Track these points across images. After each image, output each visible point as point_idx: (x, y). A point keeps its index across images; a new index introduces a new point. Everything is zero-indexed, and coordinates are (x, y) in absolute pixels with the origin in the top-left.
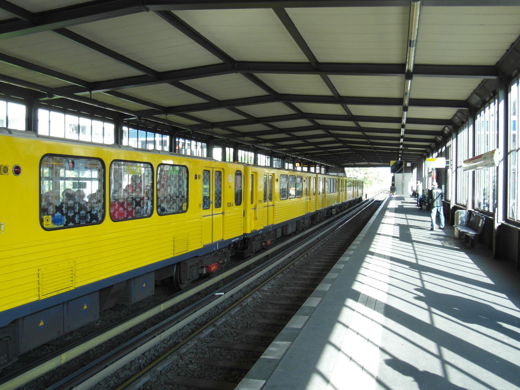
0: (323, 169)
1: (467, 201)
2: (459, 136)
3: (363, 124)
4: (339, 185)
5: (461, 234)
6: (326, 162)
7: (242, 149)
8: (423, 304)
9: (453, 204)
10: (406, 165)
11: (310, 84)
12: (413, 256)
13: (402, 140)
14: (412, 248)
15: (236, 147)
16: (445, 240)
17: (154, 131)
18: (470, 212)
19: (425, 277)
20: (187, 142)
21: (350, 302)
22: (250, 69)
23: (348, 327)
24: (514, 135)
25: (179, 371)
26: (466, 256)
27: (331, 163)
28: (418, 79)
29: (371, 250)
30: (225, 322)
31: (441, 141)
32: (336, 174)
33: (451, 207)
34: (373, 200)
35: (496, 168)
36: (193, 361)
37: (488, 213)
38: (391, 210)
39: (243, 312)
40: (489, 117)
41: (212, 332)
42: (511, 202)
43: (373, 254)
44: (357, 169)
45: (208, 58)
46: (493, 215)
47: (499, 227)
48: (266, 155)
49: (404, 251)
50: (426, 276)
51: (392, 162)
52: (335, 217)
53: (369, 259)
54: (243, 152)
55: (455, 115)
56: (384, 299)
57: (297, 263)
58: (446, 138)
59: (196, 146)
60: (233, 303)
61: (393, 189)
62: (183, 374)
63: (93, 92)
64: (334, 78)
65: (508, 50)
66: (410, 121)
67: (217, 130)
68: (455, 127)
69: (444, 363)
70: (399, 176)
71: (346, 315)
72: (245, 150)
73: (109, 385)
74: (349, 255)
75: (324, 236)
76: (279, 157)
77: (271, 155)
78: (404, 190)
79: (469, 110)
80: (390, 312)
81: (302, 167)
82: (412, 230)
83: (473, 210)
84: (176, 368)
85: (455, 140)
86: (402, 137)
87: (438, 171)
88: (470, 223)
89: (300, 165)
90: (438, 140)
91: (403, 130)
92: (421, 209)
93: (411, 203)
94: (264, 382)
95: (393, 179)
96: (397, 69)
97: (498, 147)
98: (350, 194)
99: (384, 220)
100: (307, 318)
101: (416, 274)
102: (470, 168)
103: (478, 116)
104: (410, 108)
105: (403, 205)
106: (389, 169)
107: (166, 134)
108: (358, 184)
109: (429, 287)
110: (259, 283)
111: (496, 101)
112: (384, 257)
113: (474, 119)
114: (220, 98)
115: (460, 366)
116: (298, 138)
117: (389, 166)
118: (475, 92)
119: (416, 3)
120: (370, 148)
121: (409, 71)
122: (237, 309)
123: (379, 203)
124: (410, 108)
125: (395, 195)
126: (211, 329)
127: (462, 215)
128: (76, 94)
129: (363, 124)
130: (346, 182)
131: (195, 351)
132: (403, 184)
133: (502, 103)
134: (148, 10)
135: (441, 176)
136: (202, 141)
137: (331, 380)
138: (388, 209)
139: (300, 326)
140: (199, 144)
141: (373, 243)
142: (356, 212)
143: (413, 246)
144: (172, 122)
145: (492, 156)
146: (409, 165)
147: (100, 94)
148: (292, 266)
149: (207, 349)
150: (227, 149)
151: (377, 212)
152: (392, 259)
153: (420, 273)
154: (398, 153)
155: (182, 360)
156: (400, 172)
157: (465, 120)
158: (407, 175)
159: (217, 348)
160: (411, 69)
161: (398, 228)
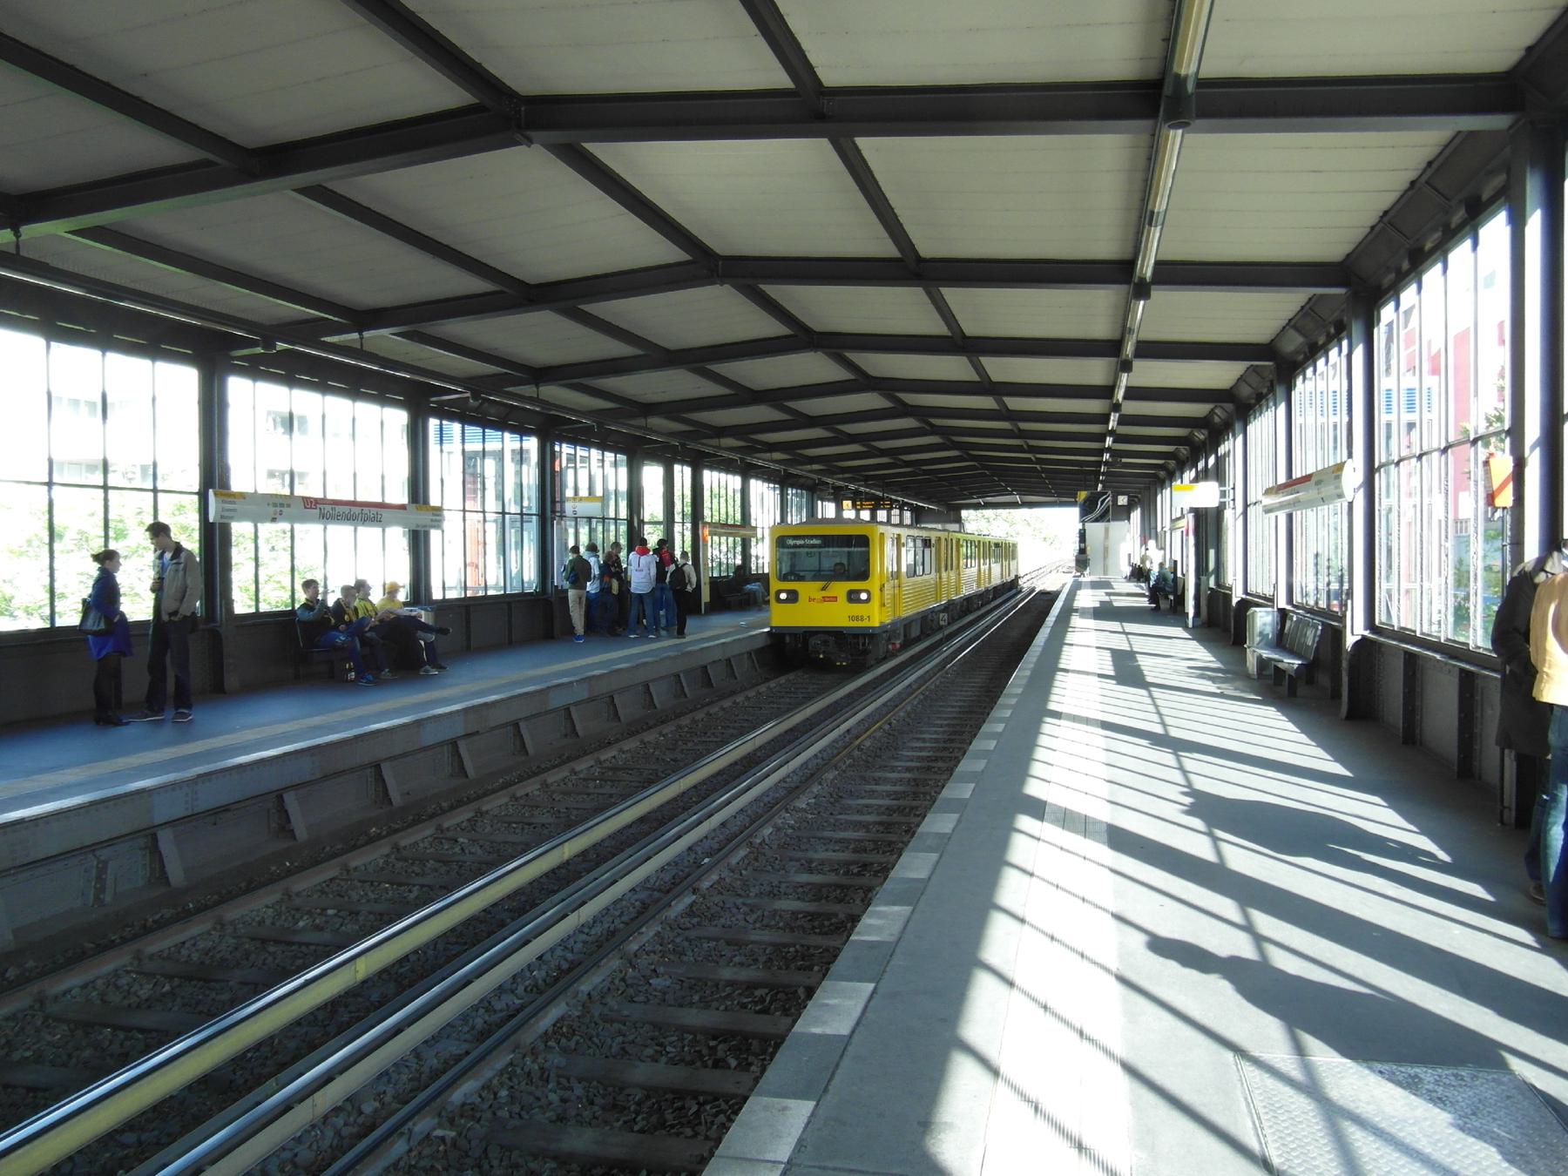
0: (907, 515)
1: (1276, 586)
2: (1250, 428)
3: (1014, 403)
4: (942, 555)
5: (1263, 663)
6: (917, 497)
7: (712, 468)
8: (1197, 823)
9: (1237, 595)
10: (1115, 500)
11: (899, 309)
12: (1156, 718)
13: (1109, 441)
14: (1149, 701)
15: (698, 463)
16: (1224, 681)
17: (501, 425)
18: (1283, 614)
19: (1189, 764)
20: (581, 452)
21: (1025, 822)
22: (751, 274)
23: (1032, 875)
24: (1389, 425)
25: (631, 991)
26: (1278, 715)
27: (928, 500)
28: (1161, 296)
29: (1052, 706)
30: (718, 882)
31: (1204, 443)
32: (939, 526)
33: (1235, 601)
34: (1033, 590)
35: (1345, 505)
36: (661, 970)
37: (1326, 614)
38: (1084, 613)
39: (756, 859)
40: (1324, 384)
41: (691, 905)
42: (1382, 587)
43: (1057, 715)
44: (989, 513)
45: (657, 250)
46: (1342, 619)
47: (1357, 644)
48: (768, 480)
49: (1130, 706)
50: (1192, 762)
51: (1083, 495)
52: (947, 632)
53: (1049, 726)
54: (715, 474)
55: (1241, 379)
56: (1104, 814)
57: (868, 744)
58: (1217, 433)
59: (603, 461)
60: (729, 841)
61: (1082, 561)
62: (641, 998)
63: (366, 334)
64: (954, 296)
65: (1373, 228)
66: (1133, 393)
67: (656, 422)
68: (1237, 408)
69: (1259, 939)
70: (1095, 529)
71: (1021, 849)
72: (720, 470)
73: (473, 1028)
74: (1000, 720)
75: (923, 680)
76: (801, 487)
77: (783, 481)
78: (1110, 562)
79: (1275, 368)
80: (1120, 840)
81: (858, 511)
82: (1143, 661)
83: (1289, 607)
84: (622, 986)
85: (1240, 439)
86: (1112, 433)
87: (1200, 515)
88: (1281, 640)
89: (854, 506)
90: (1200, 436)
91: (1114, 417)
92: (1157, 609)
93: (1133, 595)
94: (871, 986)
95: (1083, 536)
96: (1119, 272)
97: (1350, 455)
98: (973, 576)
99: (1070, 637)
100: (934, 856)
101: (1167, 757)
102: (1281, 506)
103: (1299, 380)
104: (1138, 365)
105: (1110, 602)
106: (1073, 513)
107: (529, 433)
108: (1004, 551)
109: (1201, 784)
110: (782, 792)
111: (1345, 343)
112: (1087, 721)
113: (1290, 388)
114: (671, 343)
115: (1294, 945)
116: (853, 438)
117: (1074, 504)
118: (1292, 324)
119: (1172, 132)
120: (1019, 449)
121: (1142, 279)
122: (742, 853)
123: (1048, 598)
124: (1138, 365)
125: (1088, 577)
126: (688, 899)
127: (1263, 620)
128: (328, 339)
129: (1014, 403)
130: (959, 546)
131: (659, 948)
132: (1106, 550)
133: (1359, 352)
134: (530, 142)
135: (1208, 526)
136: (616, 450)
137: (1018, 982)
138: (1076, 611)
139: (923, 875)
140: (609, 456)
141: (1055, 690)
142: (993, 622)
143: (1151, 696)
144: (547, 403)
145: (1338, 477)
146: (1123, 500)
147: (383, 339)
148: (856, 753)
149: (686, 944)
150: (677, 468)
151: (1051, 619)
152: (1106, 725)
153: (1178, 757)
154: (1098, 473)
155: (634, 967)
156: (1101, 518)
157: (1265, 391)
158: (1116, 527)
159: (709, 939)
160: (1149, 274)
161: (1108, 654)
